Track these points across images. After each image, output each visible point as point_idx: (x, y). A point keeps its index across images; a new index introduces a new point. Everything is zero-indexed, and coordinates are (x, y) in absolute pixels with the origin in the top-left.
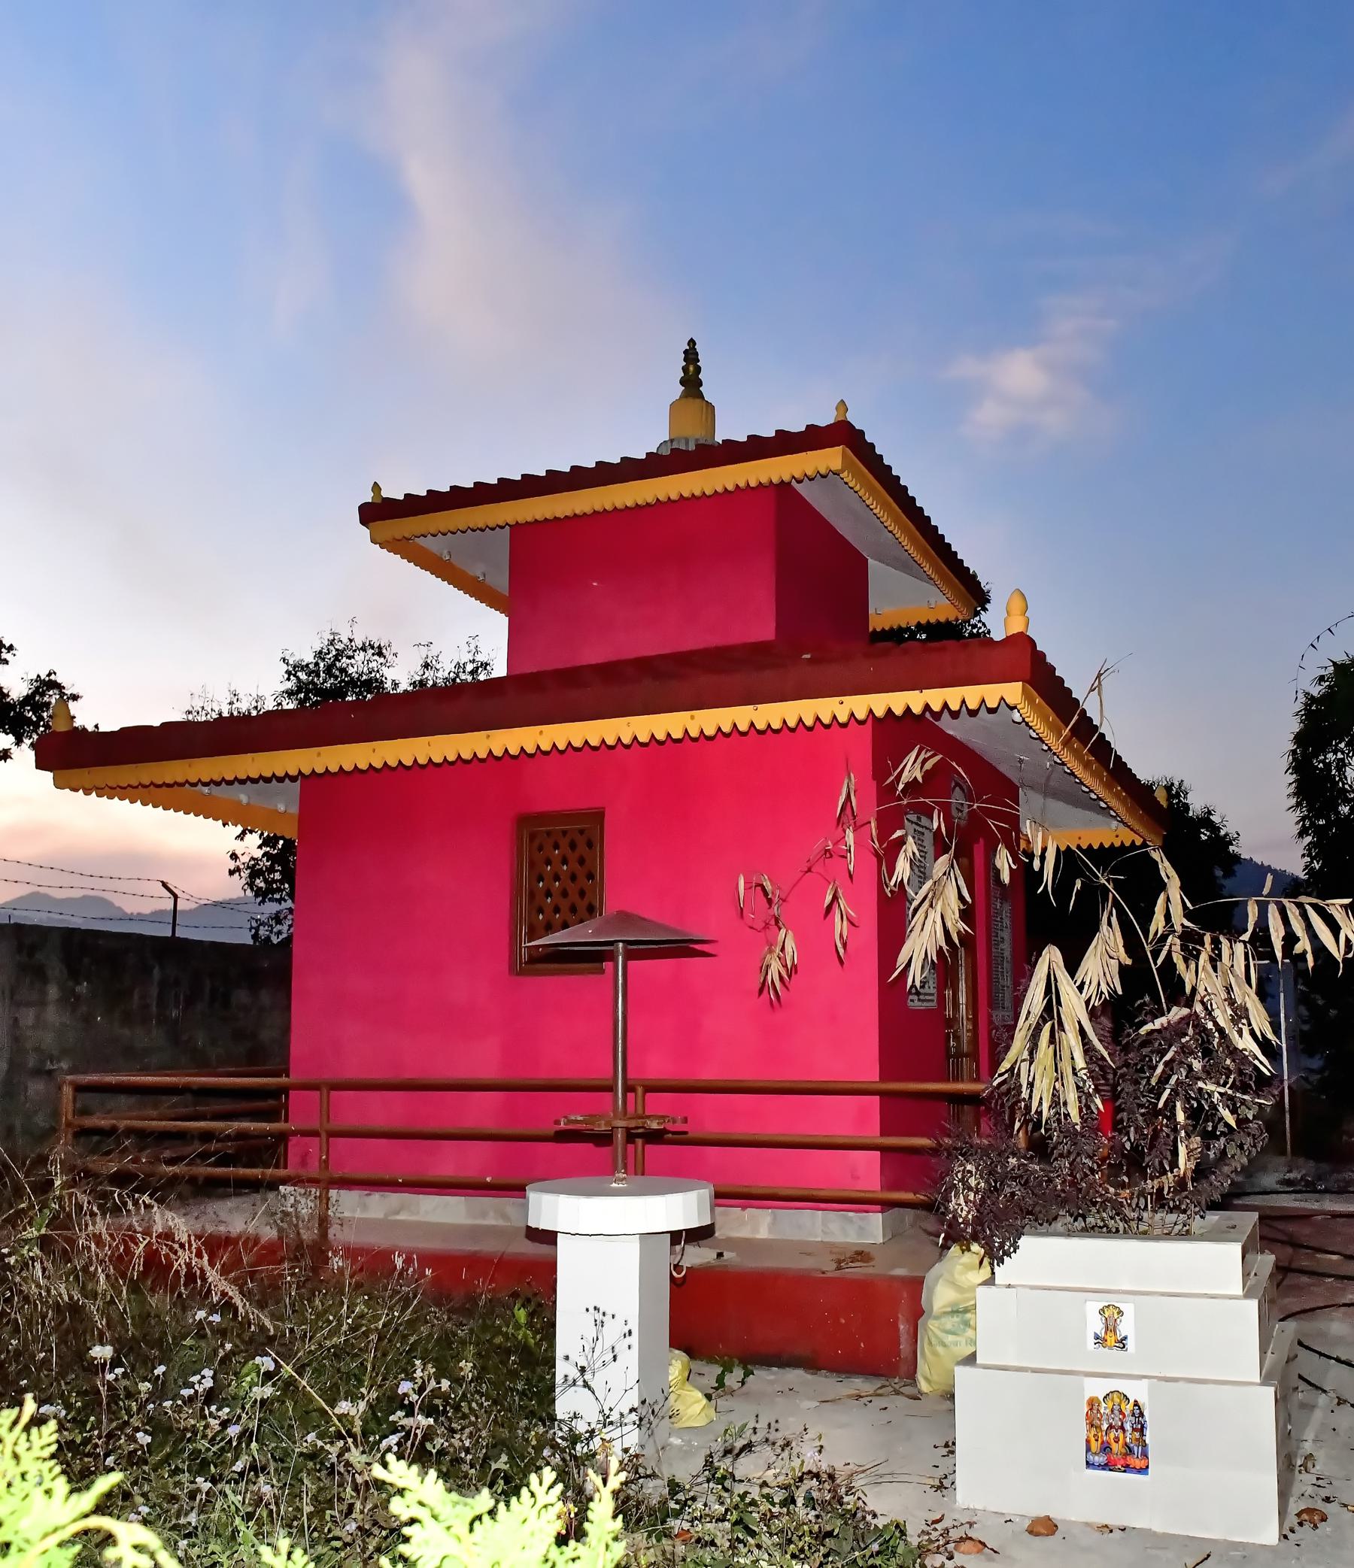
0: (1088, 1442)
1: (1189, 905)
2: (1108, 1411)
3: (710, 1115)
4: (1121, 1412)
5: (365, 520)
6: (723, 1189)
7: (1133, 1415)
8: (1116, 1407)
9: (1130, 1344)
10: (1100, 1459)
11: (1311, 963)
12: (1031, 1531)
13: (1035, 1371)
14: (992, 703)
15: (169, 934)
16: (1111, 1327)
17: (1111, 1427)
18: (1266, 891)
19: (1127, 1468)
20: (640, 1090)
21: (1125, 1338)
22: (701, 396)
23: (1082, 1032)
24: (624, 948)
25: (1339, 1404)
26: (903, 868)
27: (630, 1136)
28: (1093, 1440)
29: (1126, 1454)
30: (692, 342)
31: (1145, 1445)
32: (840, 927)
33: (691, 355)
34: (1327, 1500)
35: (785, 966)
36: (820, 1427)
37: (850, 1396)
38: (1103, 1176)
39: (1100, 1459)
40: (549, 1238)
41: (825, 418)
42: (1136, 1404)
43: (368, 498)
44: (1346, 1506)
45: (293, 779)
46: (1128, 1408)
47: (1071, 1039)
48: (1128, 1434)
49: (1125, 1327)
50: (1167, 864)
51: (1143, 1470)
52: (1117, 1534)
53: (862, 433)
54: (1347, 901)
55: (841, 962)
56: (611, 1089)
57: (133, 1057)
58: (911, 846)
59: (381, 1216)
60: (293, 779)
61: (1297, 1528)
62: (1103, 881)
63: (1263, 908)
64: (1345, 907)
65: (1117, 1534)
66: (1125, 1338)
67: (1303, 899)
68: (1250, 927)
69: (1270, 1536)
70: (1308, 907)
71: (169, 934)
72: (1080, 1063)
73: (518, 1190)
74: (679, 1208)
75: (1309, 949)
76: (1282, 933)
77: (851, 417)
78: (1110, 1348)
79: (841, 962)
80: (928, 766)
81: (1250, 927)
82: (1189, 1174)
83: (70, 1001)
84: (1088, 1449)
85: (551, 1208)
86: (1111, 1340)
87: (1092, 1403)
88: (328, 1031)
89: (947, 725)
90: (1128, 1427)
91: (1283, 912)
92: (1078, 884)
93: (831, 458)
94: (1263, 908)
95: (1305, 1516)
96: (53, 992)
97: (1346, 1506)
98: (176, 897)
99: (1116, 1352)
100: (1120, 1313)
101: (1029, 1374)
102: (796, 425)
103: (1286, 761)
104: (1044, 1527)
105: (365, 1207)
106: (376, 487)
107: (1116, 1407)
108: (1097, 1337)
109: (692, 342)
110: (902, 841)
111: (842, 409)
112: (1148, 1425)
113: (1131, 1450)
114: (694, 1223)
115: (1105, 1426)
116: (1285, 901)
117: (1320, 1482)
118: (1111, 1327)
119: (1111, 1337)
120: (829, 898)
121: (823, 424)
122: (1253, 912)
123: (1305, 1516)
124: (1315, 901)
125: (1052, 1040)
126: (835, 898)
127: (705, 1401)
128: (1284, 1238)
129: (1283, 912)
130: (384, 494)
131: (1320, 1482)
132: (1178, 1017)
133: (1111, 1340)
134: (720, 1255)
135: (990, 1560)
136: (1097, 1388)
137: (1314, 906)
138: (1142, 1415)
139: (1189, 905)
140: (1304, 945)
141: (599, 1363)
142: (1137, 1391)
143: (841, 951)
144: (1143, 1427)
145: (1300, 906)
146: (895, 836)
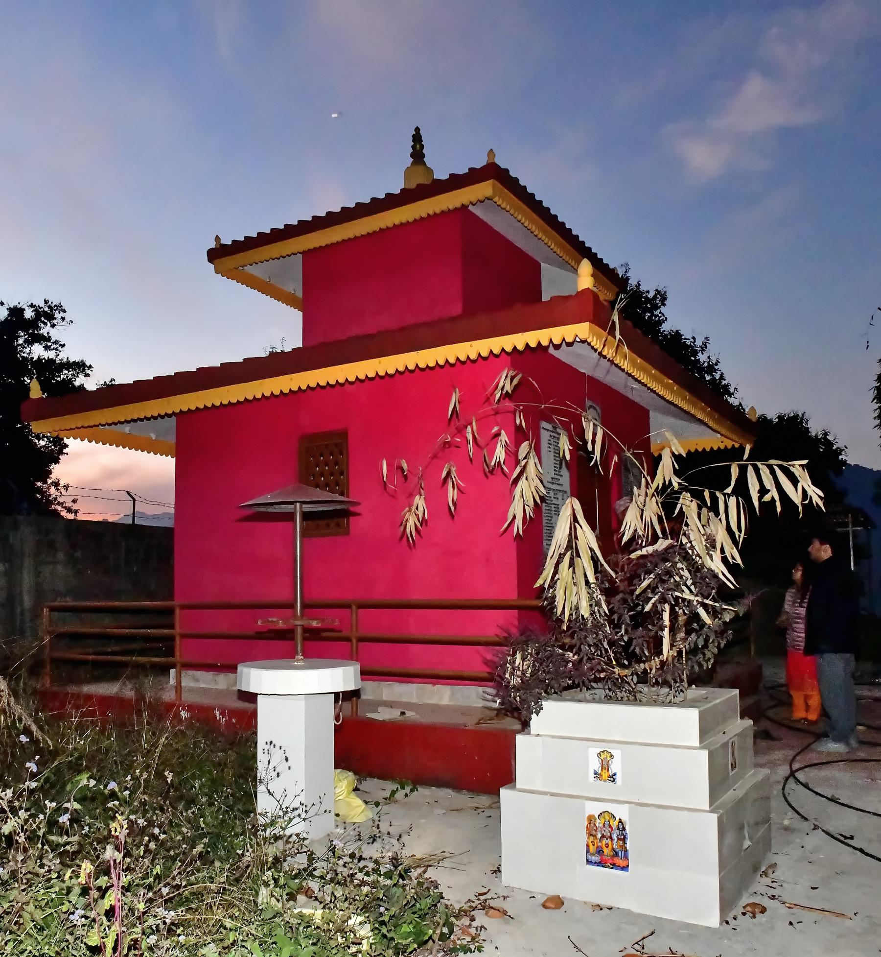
0: (588, 846)
1: (676, 466)
2: (601, 825)
3: (360, 622)
4: (610, 826)
5: (211, 259)
6: (368, 668)
7: (618, 829)
8: (607, 823)
9: (618, 778)
10: (595, 858)
11: (779, 509)
12: (544, 906)
13: (553, 795)
14: (569, 339)
15: (131, 522)
16: (605, 766)
17: (603, 836)
18: (746, 457)
19: (614, 866)
20: (354, 607)
21: (615, 774)
22: (424, 164)
23: (594, 559)
24: (301, 508)
25: (814, 829)
26: (500, 453)
27: (360, 640)
28: (591, 844)
29: (613, 856)
30: (417, 129)
31: (626, 851)
32: (452, 494)
33: (417, 138)
34: (773, 897)
35: (418, 519)
36: (426, 828)
37: (471, 808)
38: (616, 657)
39: (595, 858)
40: (252, 698)
41: (480, 162)
42: (620, 821)
43: (213, 245)
44: (784, 903)
45: (169, 416)
46: (614, 824)
47: (585, 562)
48: (614, 842)
49: (615, 767)
50: (675, 441)
51: (625, 868)
52: (605, 911)
53: (507, 171)
54: (805, 462)
55: (453, 516)
56: (292, 606)
57: (111, 594)
58: (504, 437)
59: (225, 687)
60: (169, 416)
61: (740, 917)
62: (629, 455)
63: (743, 470)
64: (802, 466)
65: (605, 911)
66: (615, 774)
67: (773, 462)
68: (733, 483)
69: (713, 920)
70: (775, 467)
71: (131, 522)
72: (592, 579)
73: (233, 669)
74: (340, 677)
75: (777, 498)
76: (757, 487)
77: (498, 161)
78: (605, 781)
79: (453, 516)
80: (515, 382)
81: (733, 483)
82: (670, 659)
83: (72, 561)
84: (588, 851)
85: (258, 678)
86: (605, 775)
87: (591, 819)
88: (197, 578)
89: (561, 355)
90: (615, 837)
91: (757, 471)
92: (616, 458)
93: (485, 189)
94: (743, 470)
95: (749, 909)
96: (61, 556)
97: (784, 903)
98: (134, 500)
99: (608, 784)
100: (612, 756)
101: (548, 797)
102: (462, 170)
103: (872, 394)
104: (555, 903)
105: (216, 683)
106: (217, 239)
107: (607, 823)
108: (596, 773)
109: (417, 129)
110: (498, 434)
111: (491, 155)
112: (628, 836)
113: (617, 854)
114: (351, 687)
115: (599, 836)
116: (759, 464)
117: (774, 885)
118: (605, 766)
119: (605, 774)
120: (444, 474)
121: (478, 167)
122: (735, 472)
123: (749, 909)
124: (780, 462)
125: (572, 564)
126: (449, 473)
127: (364, 806)
128: (324, 634)
129: (757, 471)
130: (222, 242)
131: (774, 885)
132: (664, 546)
133: (605, 775)
134: (403, 713)
135: (507, 923)
136: (595, 809)
137: (781, 467)
138: (624, 829)
139: (676, 466)
140: (774, 493)
141: (269, 778)
142: (621, 812)
143: (453, 508)
144: (625, 837)
145: (770, 467)
146: (493, 431)
